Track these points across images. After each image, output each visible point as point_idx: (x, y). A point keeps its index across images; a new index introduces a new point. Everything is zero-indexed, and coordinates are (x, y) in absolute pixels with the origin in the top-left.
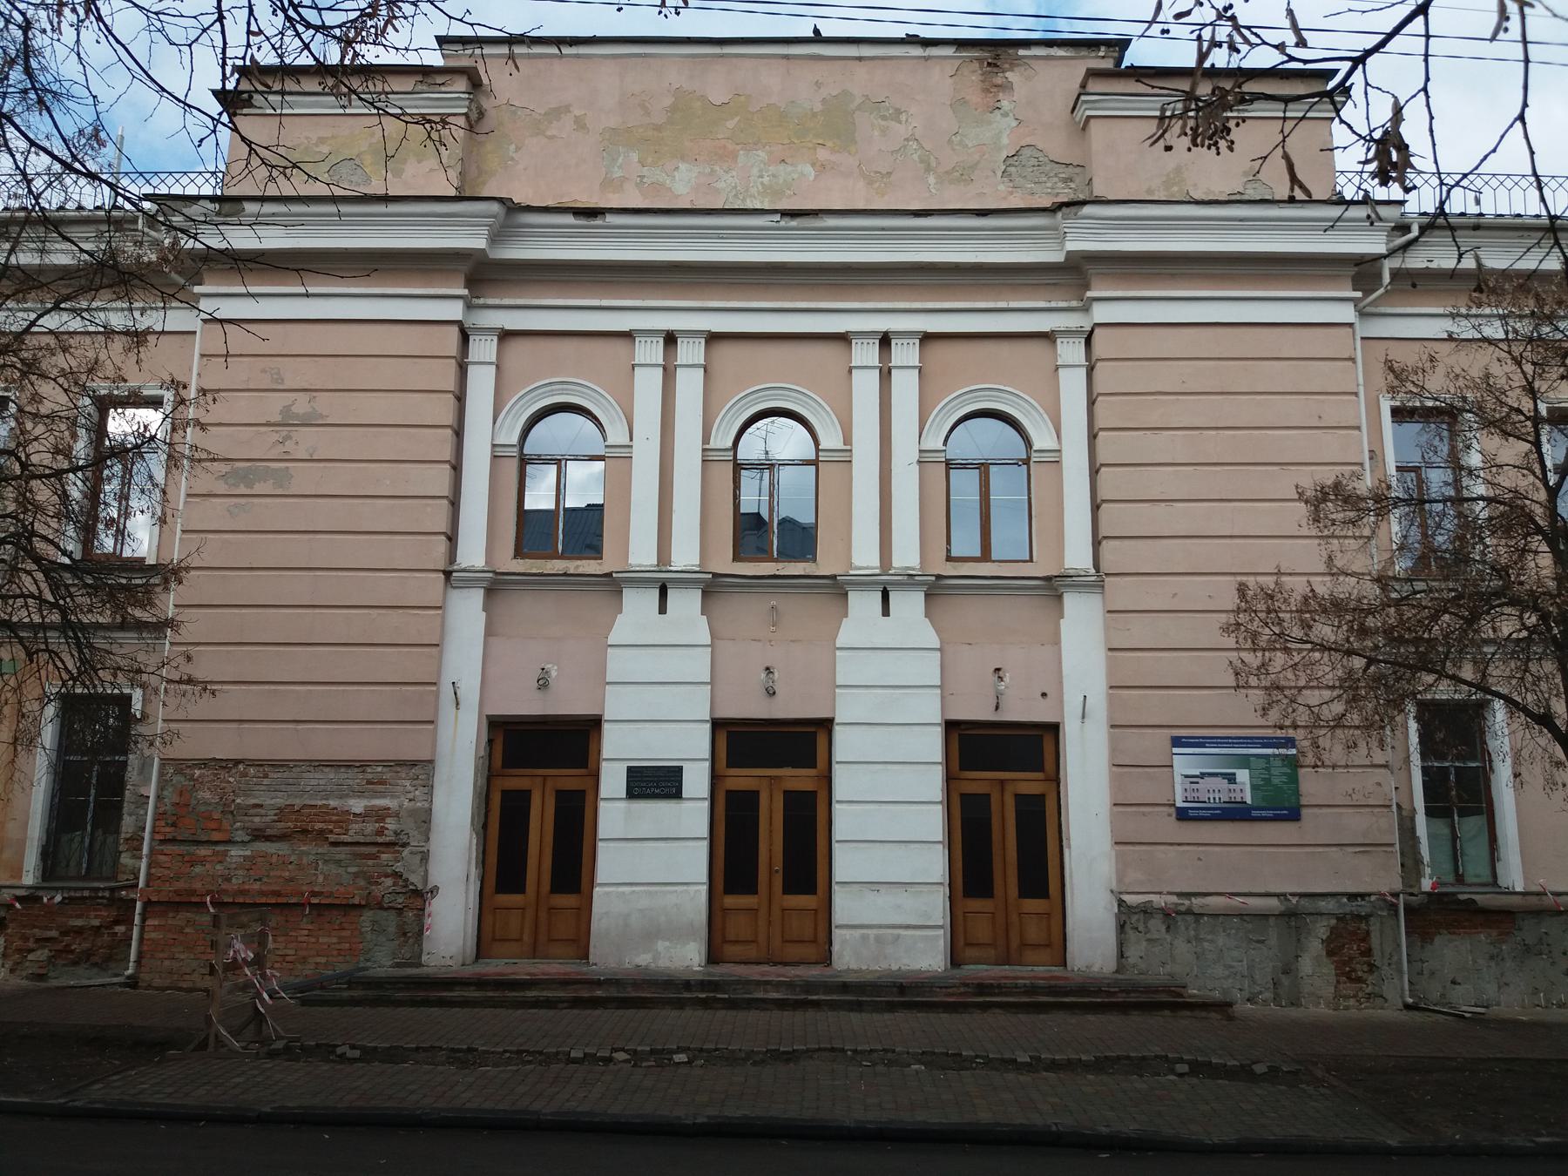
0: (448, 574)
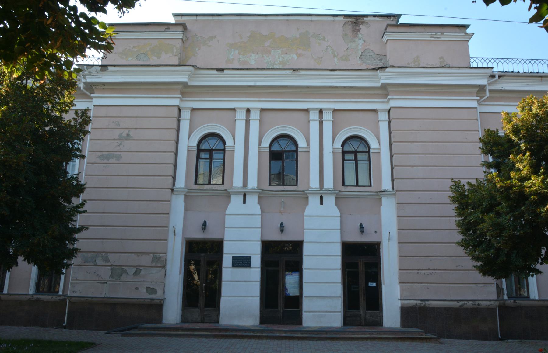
0: (172, 190)
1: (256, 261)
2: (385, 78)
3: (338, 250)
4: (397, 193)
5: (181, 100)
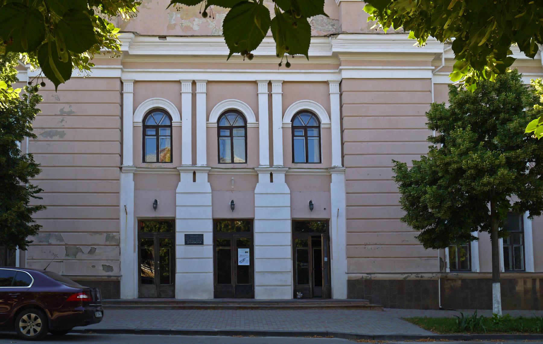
1: (209, 239)
5: (123, 71)
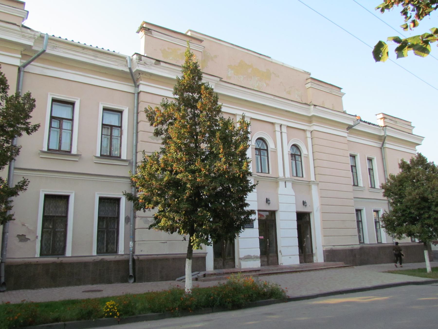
2: (312, 112)
3: (294, 217)
4: (320, 183)
